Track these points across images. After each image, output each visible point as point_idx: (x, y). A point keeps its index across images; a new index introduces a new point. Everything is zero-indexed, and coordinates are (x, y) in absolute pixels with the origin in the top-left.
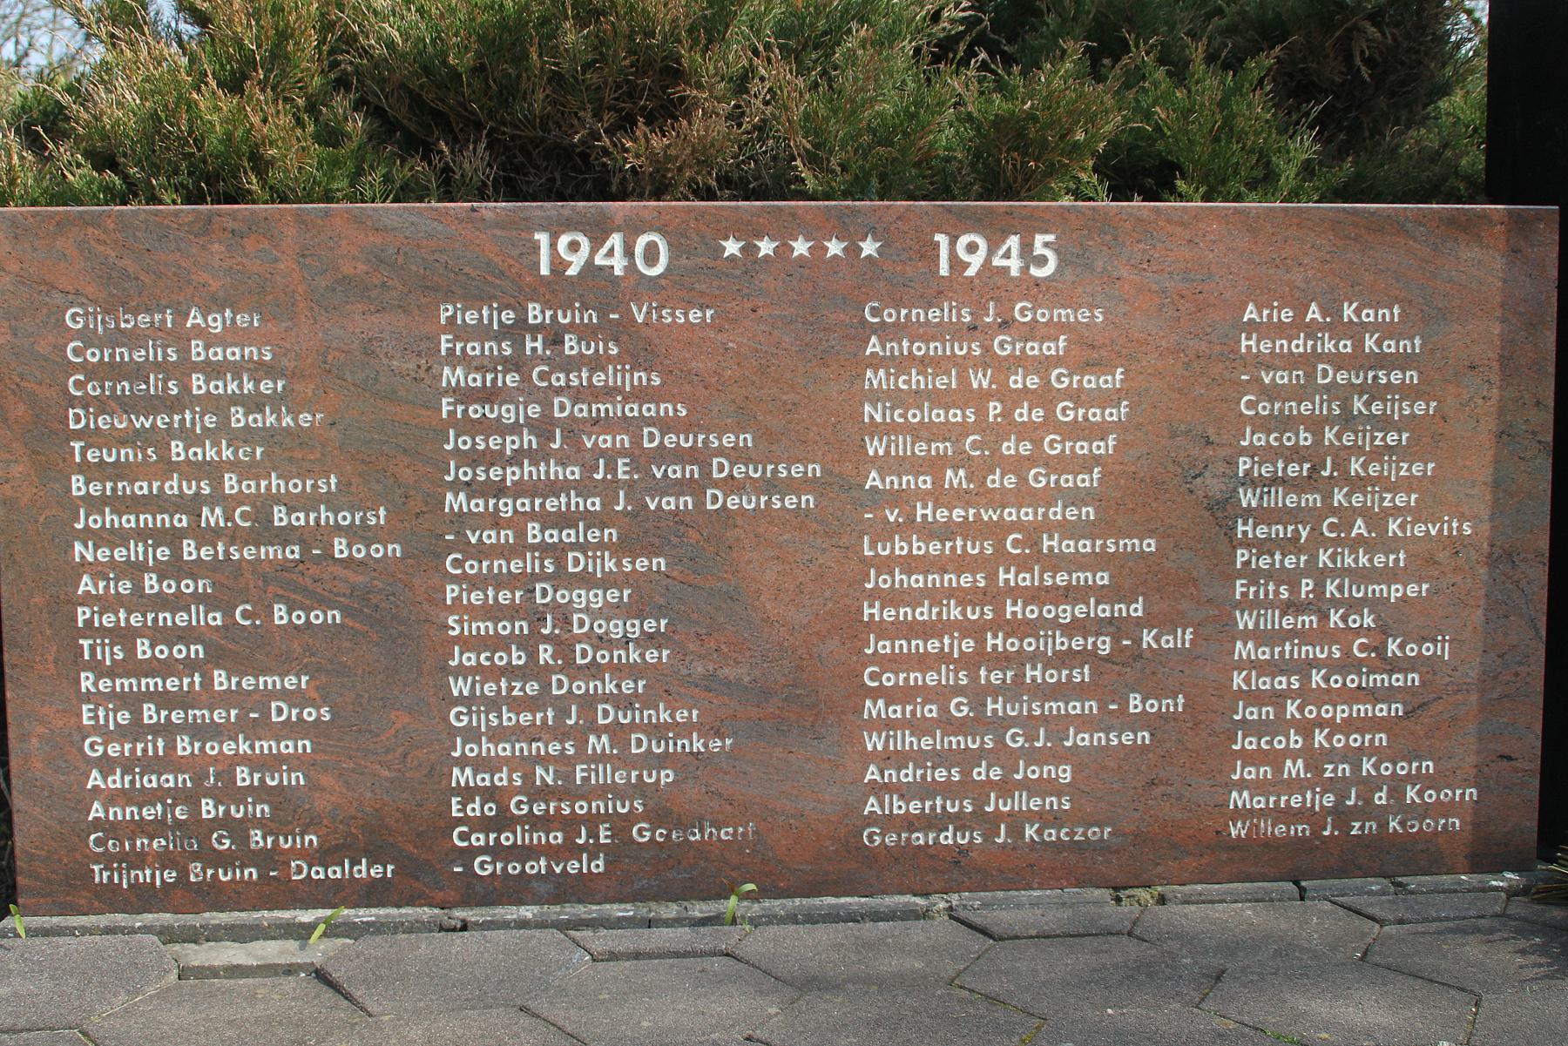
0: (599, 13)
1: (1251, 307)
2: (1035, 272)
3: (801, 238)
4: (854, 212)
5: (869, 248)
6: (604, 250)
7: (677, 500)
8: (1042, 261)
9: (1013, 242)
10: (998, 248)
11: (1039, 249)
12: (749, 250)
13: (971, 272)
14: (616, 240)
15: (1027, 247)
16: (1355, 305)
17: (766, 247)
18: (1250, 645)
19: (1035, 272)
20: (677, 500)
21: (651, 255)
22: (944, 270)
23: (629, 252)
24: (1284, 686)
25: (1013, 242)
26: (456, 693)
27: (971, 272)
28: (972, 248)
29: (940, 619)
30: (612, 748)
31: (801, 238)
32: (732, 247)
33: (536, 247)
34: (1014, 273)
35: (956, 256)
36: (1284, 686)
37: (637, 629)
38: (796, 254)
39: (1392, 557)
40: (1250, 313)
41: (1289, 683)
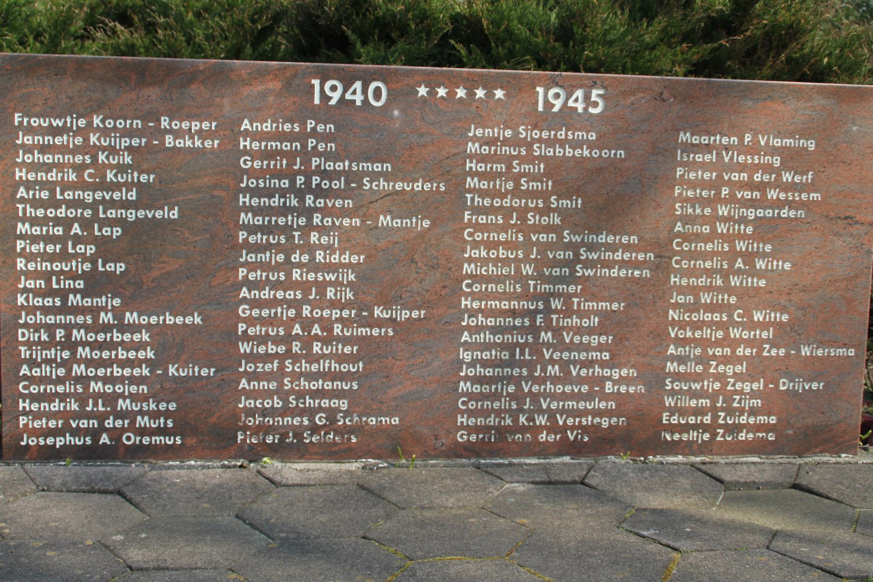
0: (231, 7)
1: (246, 121)
2: (591, 110)
3: (480, 88)
4: (520, 76)
5: (499, 94)
6: (351, 90)
7: (54, 156)
8: (595, 105)
9: (579, 93)
10: (571, 96)
11: (594, 98)
12: (432, 93)
13: (333, 102)
14: (358, 85)
15: (587, 97)
16: (101, 117)
17: (442, 92)
18: (675, 364)
19: (591, 110)
20: (54, 156)
21: (377, 93)
22: (317, 101)
23: (365, 92)
24: (292, 297)
25: (579, 93)
26: (553, 307)
27: (333, 102)
28: (557, 96)
29: (829, 355)
30: (82, 232)
31: (480, 88)
32: (423, 91)
33: (313, 86)
34: (580, 110)
35: (549, 101)
36: (292, 297)
37: (91, 198)
38: (419, 95)
39: (752, 333)
40: (246, 125)
41: (295, 295)
